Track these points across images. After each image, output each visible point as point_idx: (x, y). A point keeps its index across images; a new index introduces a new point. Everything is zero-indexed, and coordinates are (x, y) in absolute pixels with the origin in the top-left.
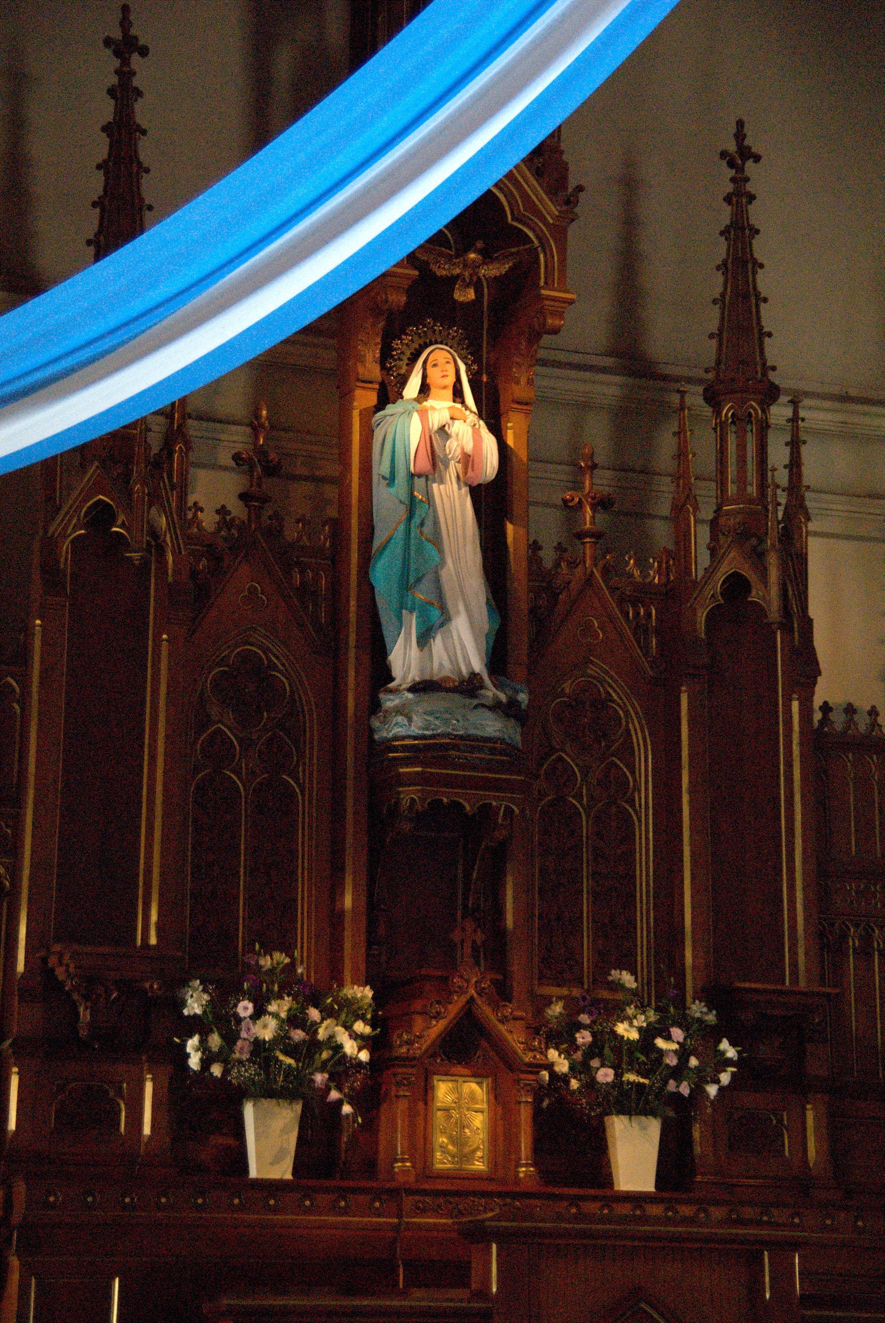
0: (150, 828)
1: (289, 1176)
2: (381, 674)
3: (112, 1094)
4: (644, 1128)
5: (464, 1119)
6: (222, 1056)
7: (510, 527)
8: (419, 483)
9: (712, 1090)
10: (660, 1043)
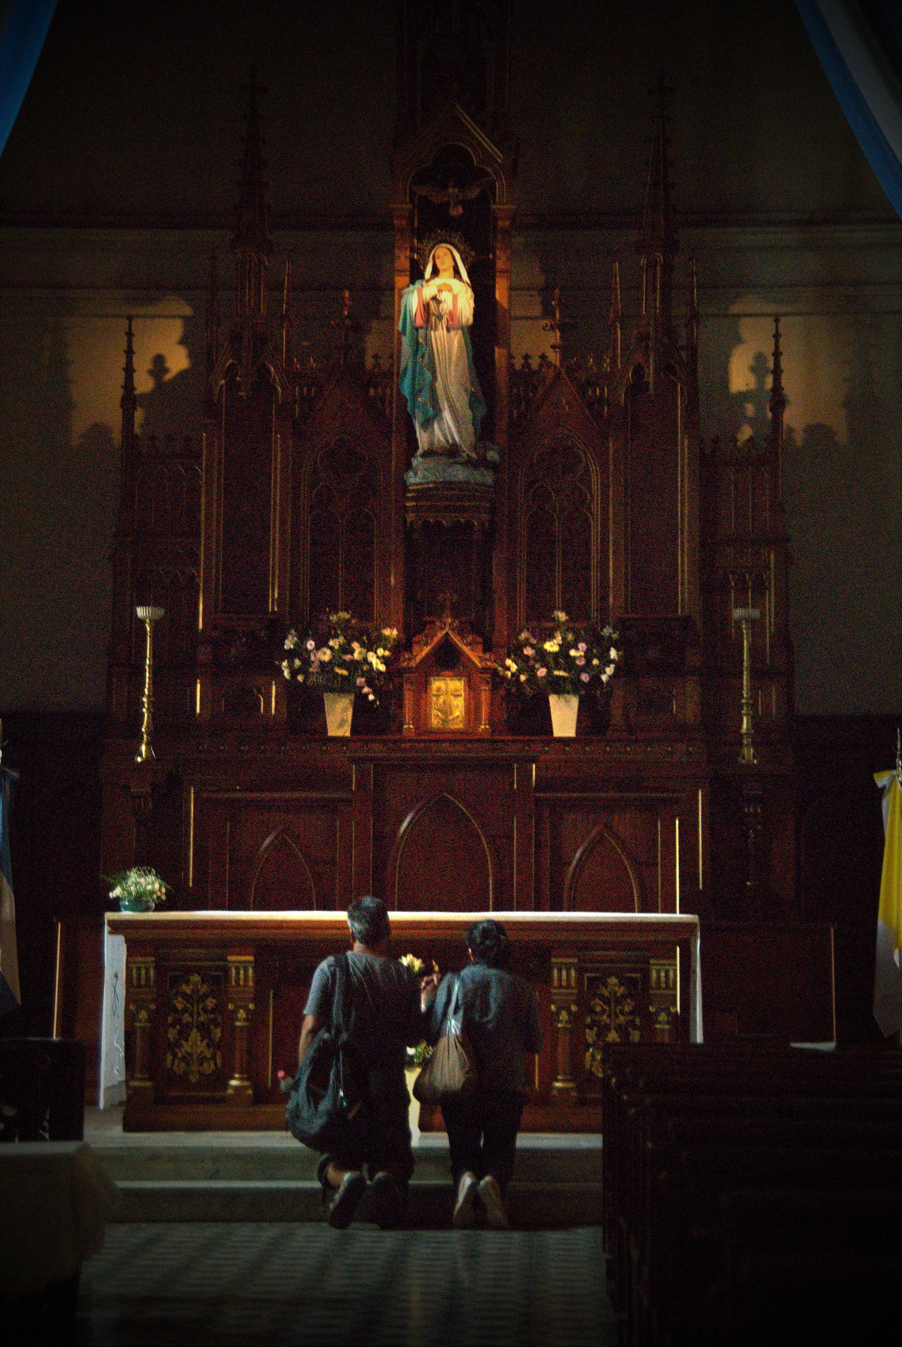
1: (348, 734)
2: (413, 443)
3: (744, 712)
4: (567, 701)
5: (449, 700)
6: (300, 671)
7: (496, 349)
9: (604, 678)
10: (573, 653)
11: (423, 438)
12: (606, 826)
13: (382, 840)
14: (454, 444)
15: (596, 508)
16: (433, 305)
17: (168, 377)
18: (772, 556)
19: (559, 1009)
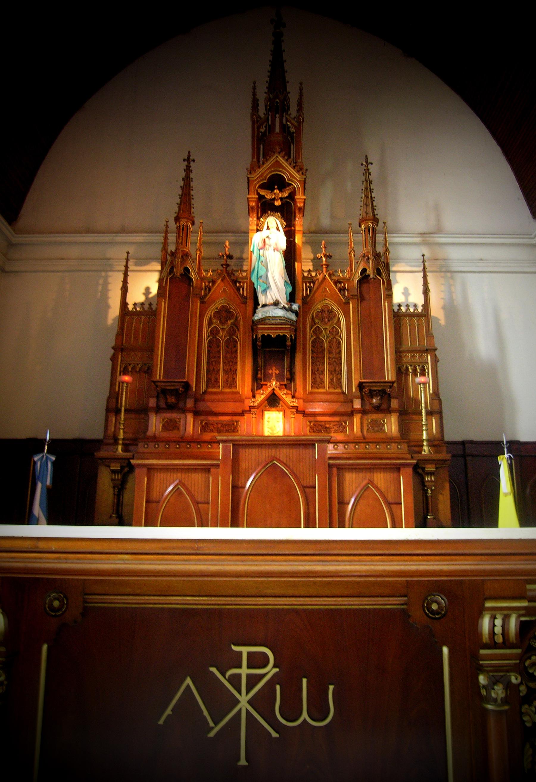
0: (162, 342)
7: (296, 264)
8: (262, 251)
11: (262, 299)
12: (369, 480)
13: (236, 488)
14: (277, 300)
15: (344, 336)
16: (267, 240)
17: (151, 296)
18: (429, 358)
19: (494, 682)
